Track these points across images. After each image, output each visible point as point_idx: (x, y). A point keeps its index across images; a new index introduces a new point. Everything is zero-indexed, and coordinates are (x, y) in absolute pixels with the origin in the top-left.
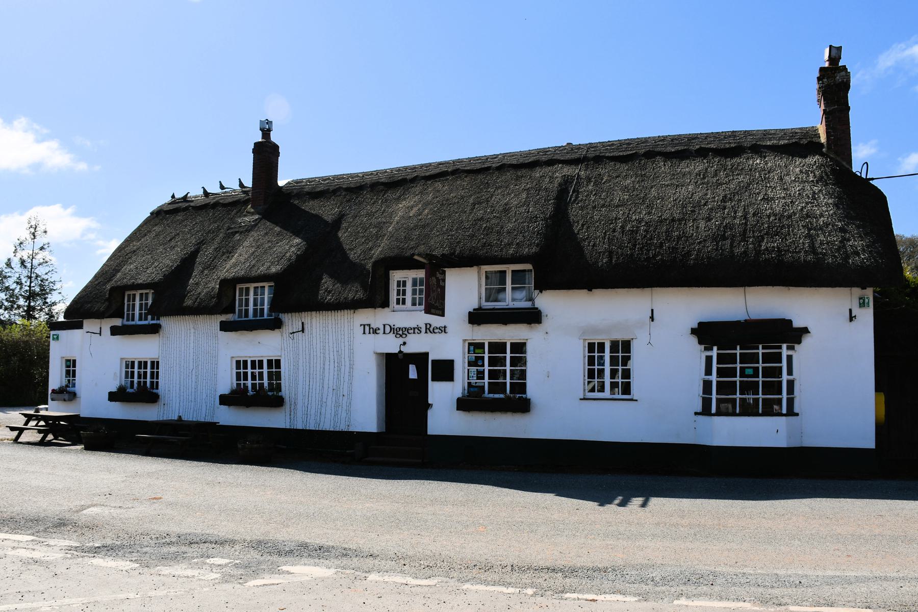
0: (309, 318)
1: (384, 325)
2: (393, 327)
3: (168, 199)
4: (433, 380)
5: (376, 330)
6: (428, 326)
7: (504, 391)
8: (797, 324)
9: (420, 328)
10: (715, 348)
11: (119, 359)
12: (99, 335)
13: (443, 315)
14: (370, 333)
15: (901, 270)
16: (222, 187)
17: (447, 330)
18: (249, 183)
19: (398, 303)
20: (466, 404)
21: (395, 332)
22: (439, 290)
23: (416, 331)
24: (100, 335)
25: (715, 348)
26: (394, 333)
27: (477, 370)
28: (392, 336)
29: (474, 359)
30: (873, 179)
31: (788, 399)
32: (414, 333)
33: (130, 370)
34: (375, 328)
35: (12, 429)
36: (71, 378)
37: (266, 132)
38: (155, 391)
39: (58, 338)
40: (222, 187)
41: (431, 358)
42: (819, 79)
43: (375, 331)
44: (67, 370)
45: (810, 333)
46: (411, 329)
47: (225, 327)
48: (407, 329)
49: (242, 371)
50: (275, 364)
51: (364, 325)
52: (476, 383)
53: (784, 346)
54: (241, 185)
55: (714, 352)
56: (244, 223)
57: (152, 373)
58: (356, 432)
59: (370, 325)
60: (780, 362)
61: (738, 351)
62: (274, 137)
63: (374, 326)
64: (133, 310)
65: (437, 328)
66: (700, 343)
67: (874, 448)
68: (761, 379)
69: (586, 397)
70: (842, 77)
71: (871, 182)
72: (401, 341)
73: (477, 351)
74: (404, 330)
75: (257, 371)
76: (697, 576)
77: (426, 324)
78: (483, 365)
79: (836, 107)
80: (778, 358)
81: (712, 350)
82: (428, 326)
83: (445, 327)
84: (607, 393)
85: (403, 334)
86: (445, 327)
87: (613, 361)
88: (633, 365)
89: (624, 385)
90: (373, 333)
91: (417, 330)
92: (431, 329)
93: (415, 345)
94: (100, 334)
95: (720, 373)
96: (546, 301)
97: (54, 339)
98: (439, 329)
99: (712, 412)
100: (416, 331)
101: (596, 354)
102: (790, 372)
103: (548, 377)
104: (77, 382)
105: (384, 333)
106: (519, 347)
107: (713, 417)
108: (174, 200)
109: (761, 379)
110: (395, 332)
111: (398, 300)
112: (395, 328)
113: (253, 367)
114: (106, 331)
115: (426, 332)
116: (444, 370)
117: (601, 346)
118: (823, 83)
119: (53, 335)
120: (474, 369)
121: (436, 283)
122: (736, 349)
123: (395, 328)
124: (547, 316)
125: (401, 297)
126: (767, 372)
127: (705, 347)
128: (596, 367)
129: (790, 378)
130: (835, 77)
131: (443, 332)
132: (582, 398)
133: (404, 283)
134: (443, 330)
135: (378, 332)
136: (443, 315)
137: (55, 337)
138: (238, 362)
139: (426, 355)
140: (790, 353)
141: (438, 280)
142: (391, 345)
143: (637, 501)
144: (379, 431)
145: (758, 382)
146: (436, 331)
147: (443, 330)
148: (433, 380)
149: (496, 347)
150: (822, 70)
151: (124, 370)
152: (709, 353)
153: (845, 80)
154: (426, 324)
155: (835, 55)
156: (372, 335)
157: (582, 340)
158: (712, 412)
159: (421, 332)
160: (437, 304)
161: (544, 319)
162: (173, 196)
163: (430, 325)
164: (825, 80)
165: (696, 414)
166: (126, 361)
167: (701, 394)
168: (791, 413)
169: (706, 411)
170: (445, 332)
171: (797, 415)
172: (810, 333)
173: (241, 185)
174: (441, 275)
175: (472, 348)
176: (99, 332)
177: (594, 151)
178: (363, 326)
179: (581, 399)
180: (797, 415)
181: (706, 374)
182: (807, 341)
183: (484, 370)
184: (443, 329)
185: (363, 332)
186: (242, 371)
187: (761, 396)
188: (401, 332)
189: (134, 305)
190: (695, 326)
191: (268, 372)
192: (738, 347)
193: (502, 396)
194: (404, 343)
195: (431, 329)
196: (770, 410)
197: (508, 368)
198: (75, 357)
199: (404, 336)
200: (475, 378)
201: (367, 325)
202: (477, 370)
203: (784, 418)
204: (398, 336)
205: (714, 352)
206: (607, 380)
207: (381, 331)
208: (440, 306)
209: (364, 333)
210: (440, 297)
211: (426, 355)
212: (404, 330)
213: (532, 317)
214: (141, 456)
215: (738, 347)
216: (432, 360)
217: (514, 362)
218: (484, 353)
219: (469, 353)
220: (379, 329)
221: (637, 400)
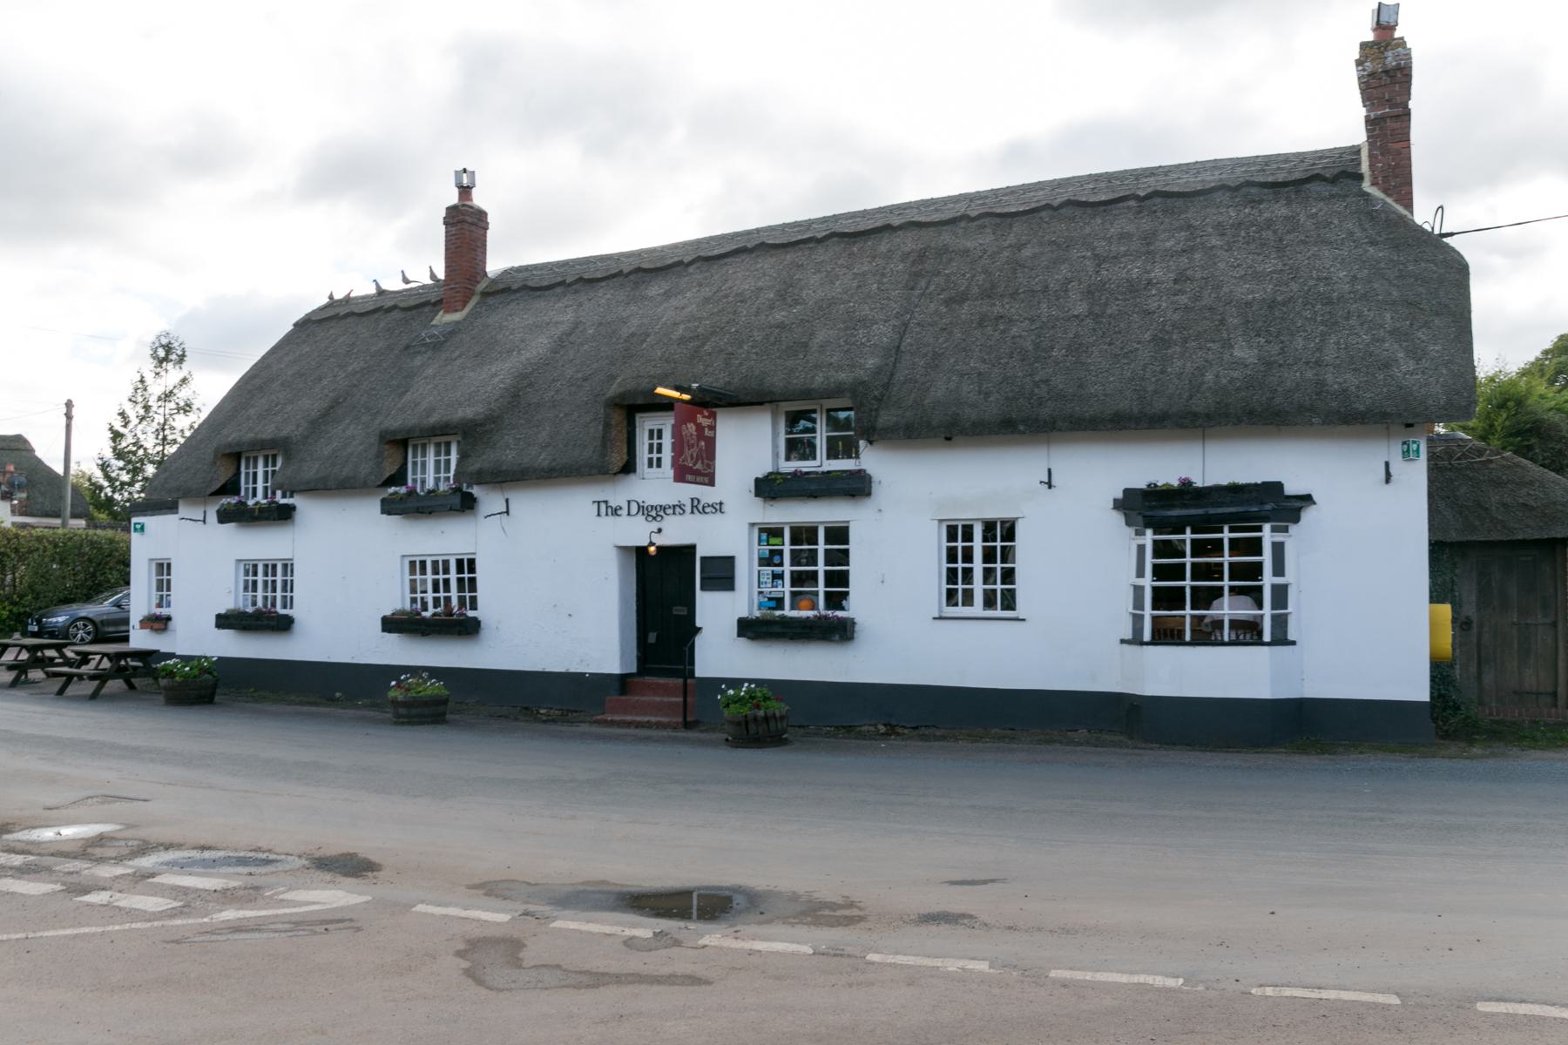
1: (629, 502)
2: (642, 504)
3: (325, 301)
4: (703, 589)
5: (616, 510)
6: (696, 503)
7: (814, 607)
8: (1290, 489)
9: (682, 507)
11: (234, 562)
12: (1046, 486)
13: (712, 483)
14: (607, 515)
15: (706, 445)
16: (406, 281)
17: (725, 508)
18: (441, 275)
19: (650, 465)
20: (748, 628)
21: (646, 512)
22: (703, 444)
23: (678, 510)
24: (508, 514)
26: (643, 514)
27: (773, 571)
28: (641, 518)
29: (767, 554)
30: (1451, 234)
31: (1274, 617)
32: (674, 513)
33: (466, 575)
34: (614, 506)
36: (165, 593)
37: (465, 191)
38: (471, 614)
39: (142, 529)
40: (406, 281)
41: (699, 554)
42: (1359, 63)
43: (615, 512)
44: (158, 580)
45: (1315, 503)
46: (670, 507)
47: (225, 517)
48: (664, 508)
50: (467, 565)
51: (599, 502)
52: (771, 592)
53: (1267, 527)
54: (433, 276)
56: (429, 337)
57: (285, 582)
58: (590, 674)
59: (606, 502)
60: (1260, 553)
62: (479, 199)
63: (613, 504)
64: (255, 482)
65: (709, 506)
66: (1128, 524)
67: (1427, 699)
69: (944, 615)
70: (1398, 58)
71: (1444, 240)
72: (654, 526)
73: (772, 541)
74: (659, 509)
75: (441, 577)
77: (692, 499)
78: (781, 564)
79: (1387, 110)
80: (1255, 547)
81: (1144, 534)
82: (696, 503)
83: (721, 504)
84: (978, 608)
85: (658, 515)
86: (721, 504)
87: (989, 556)
88: (1021, 565)
90: (612, 514)
91: (677, 508)
92: (700, 508)
93: (674, 533)
94: (204, 521)
95: (1159, 572)
96: (871, 460)
97: (136, 530)
98: (712, 506)
100: (678, 510)
101: (999, 544)
102: (1279, 569)
103: (883, 582)
104: (172, 598)
105: (629, 514)
106: (839, 534)
107: (1145, 647)
108: (332, 303)
110: (646, 512)
111: (650, 461)
112: (645, 506)
113: (460, 569)
114: (212, 517)
115: (692, 512)
116: (721, 574)
118: (1364, 70)
119: (135, 524)
120: (769, 569)
121: (695, 433)
122: (1184, 533)
123: (645, 506)
124: (880, 482)
125: (655, 456)
126: (1237, 571)
127: (1272, 526)
128: (999, 566)
129: (1279, 580)
130: (1386, 58)
131: (718, 511)
132: (937, 616)
133: (660, 432)
134: (718, 508)
135: (619, 512)
136: (712, 483)
137: (138, 527)
138: (412, 563)
139: (691, 549)
140: (1279, 537)
141: (700, 428)
142: (638, 533)
144: (624, 672)
146: (707, 510)
147: (718, 508)
148: (703, 589)
149: (803, 534)
150: (1364, 46)
151: (242, 578)
152: (1140, 541)
153: (1403, 62)
154: (692, 499)
155: (1384, 26)
156: (611, 519)
157: (936, 522)
159: (684, 511)
160: (699, 466)
161: (875, 488)
162: (331, 297)
163: (699, 501)
164: (1368, 64)
165: (1123, 641)
166: (245, 565)
167: (1131, 609)
168: (1281, 639)
169: (1136, 640)
170: (721, 511)
171: (1293, 643)
172: (1315, 503)
173: (433, 276)
174: (706, 420)
175: (764, 536)
176: (202, 518)
177: (982, 205)
178: (596, 504)
179: (935, 618)
180: (1293, 643)
182: (1308, 515)
183: (783, 571)
184: (718, 507)
185: (596, 513)
188: (654, 513)
189: (255, 474)
190: (1120, 495)
193: (811, 614)
194: (660, 531)
195: (700, 508)
196: (1248, 633)
198: (169, 559)
199: (659, 519)
200: (770, 586)
201: (604, 501)
202: (773, 571)
203: (1266, 648)
204: (650, 519)
205: (1149, 537)
206: (978, 587)
207: (624, 512)
208: (704, 470)
209: (599, 515)
210: (704, 455)
211: (691, 549)
212: (659, 509)
213: (857, 487)
214: (729, 748)
217: (831, 558)
218: (783, 545)
219: (759, 545)
220: (621, 508)
221: (1024, 620)
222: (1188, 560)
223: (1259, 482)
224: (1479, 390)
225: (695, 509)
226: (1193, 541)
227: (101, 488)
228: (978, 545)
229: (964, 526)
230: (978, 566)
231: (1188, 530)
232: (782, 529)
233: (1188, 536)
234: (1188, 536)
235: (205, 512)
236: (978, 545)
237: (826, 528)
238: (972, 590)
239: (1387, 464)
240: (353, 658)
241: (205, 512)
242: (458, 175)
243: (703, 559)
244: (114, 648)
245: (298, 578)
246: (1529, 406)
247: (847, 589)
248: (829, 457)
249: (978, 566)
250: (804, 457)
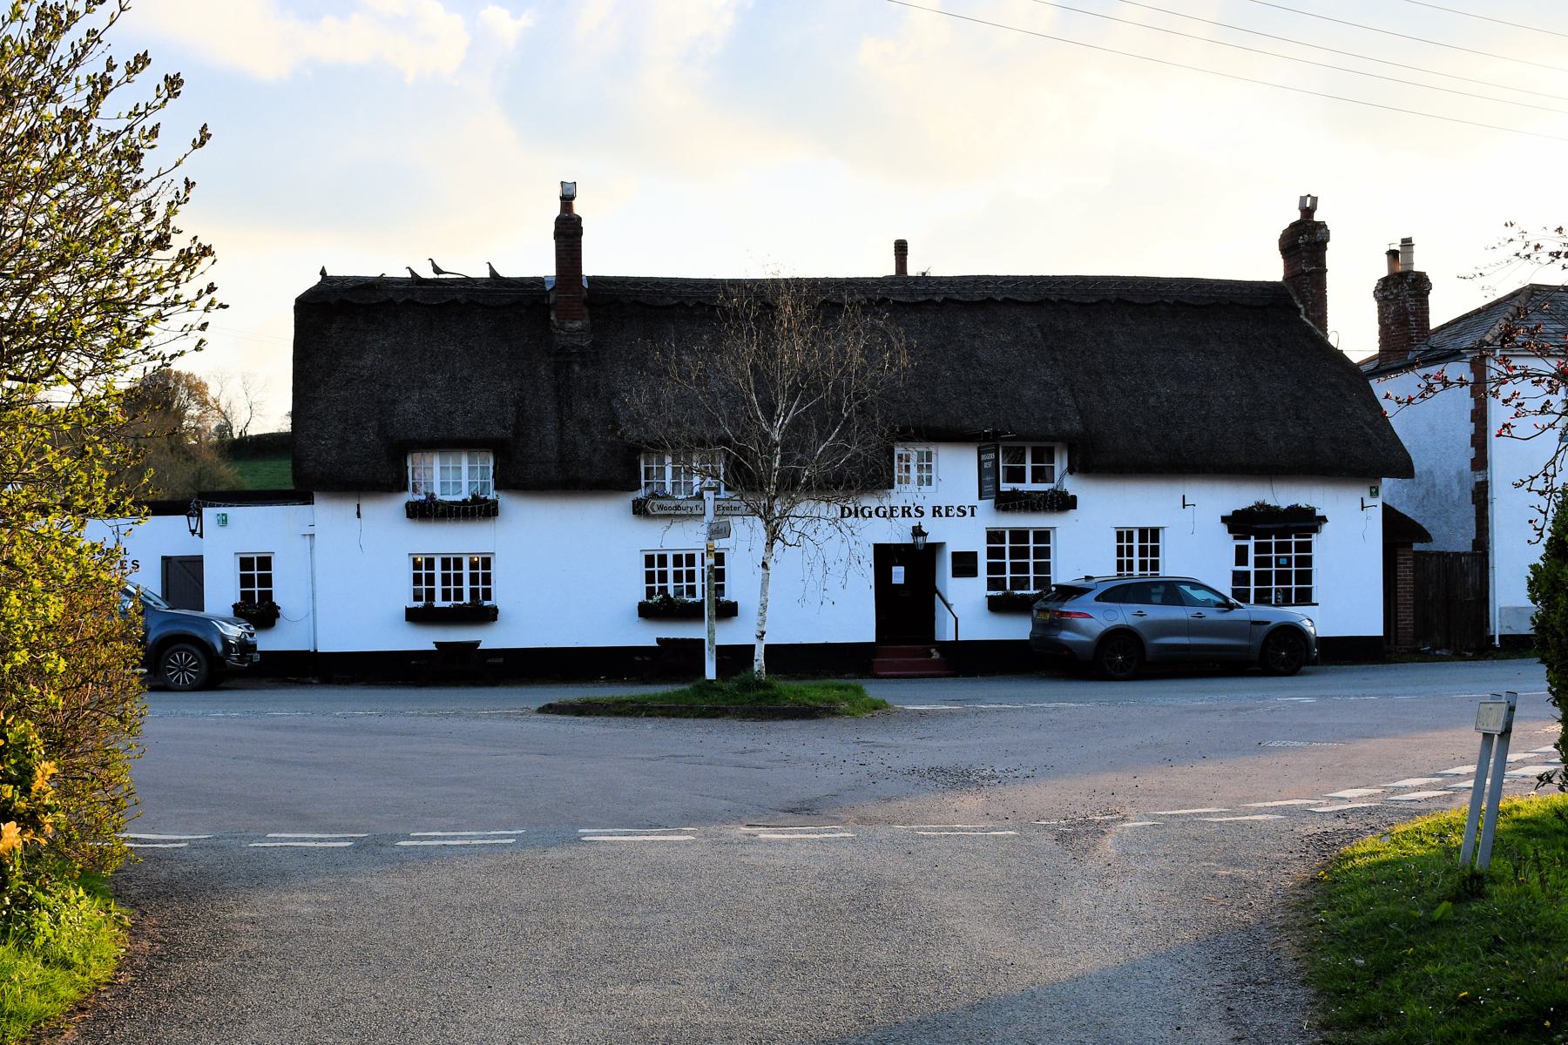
0: (261, 904)
7: (1004, 588)
10: (1253, 537)
25: (1253, 537)
35: (1521, 480)
49: (1125, 544)
55: (1251, 543)
61: (1293, 540)
68: (1294, 568)
76: (79, 53)
81: (1250, 539)
87: (1143, 551)
89: (1027, 586)
99: (1498, 626)
106: (1043, 536)
109: (1294, 568)
117: (663, 560)
126: (1267, 562)
143: (279, 611)
145: (483, 584)
149: (1019, 535)
158: (1498, 626)
166: (471, 558)
181: (1237, 564)
186: (1125, 544)
187: (1293, 586)
191: (443, 574)
192: (1273, 537)
197: (1031, 575)
213: (1065, 503)
215: (1273, 537)
216: (953, 553)
222: (1293, 554)
223: (1240, 509)
224: (185, 423)
225: (906, 514)
226: (1296, 542)
227: (29, 469)
228: (1136, 544)
229: (1127, 532)
230: (1136, 559)
231: (1293, 536)
232: (1028, 532)
233: (1273, 540)
234: (1273, 540)
235: (358, 506)
236: (1136, 544)
237: (1034, 532)
238: (443, 569)
239: (1362, 499)
240: (577, 643)
241: (358, 506)
242: (1303, 199)
243: (955, 555)
244: (1070, 637)
245: (276, 572)
246: (926, 463)
247: (647, 569)
248: (1033, 482)
249: (1136, 559)
250: (1044, 480)
